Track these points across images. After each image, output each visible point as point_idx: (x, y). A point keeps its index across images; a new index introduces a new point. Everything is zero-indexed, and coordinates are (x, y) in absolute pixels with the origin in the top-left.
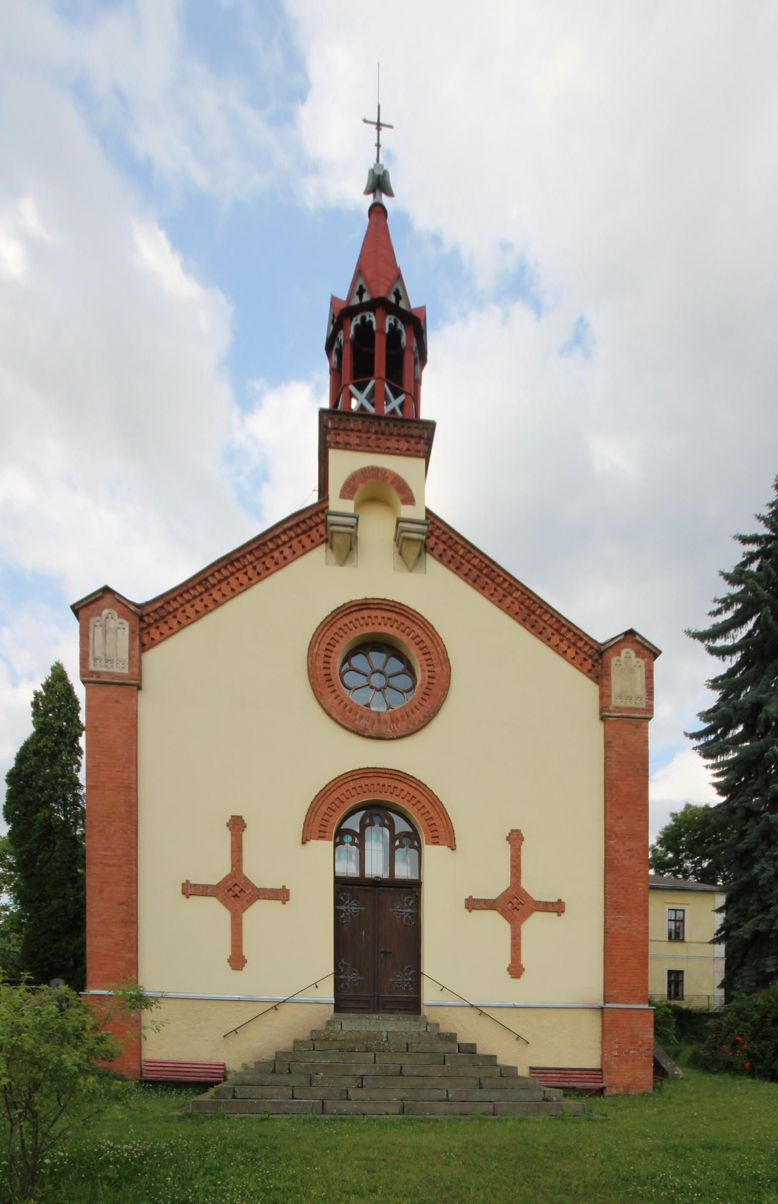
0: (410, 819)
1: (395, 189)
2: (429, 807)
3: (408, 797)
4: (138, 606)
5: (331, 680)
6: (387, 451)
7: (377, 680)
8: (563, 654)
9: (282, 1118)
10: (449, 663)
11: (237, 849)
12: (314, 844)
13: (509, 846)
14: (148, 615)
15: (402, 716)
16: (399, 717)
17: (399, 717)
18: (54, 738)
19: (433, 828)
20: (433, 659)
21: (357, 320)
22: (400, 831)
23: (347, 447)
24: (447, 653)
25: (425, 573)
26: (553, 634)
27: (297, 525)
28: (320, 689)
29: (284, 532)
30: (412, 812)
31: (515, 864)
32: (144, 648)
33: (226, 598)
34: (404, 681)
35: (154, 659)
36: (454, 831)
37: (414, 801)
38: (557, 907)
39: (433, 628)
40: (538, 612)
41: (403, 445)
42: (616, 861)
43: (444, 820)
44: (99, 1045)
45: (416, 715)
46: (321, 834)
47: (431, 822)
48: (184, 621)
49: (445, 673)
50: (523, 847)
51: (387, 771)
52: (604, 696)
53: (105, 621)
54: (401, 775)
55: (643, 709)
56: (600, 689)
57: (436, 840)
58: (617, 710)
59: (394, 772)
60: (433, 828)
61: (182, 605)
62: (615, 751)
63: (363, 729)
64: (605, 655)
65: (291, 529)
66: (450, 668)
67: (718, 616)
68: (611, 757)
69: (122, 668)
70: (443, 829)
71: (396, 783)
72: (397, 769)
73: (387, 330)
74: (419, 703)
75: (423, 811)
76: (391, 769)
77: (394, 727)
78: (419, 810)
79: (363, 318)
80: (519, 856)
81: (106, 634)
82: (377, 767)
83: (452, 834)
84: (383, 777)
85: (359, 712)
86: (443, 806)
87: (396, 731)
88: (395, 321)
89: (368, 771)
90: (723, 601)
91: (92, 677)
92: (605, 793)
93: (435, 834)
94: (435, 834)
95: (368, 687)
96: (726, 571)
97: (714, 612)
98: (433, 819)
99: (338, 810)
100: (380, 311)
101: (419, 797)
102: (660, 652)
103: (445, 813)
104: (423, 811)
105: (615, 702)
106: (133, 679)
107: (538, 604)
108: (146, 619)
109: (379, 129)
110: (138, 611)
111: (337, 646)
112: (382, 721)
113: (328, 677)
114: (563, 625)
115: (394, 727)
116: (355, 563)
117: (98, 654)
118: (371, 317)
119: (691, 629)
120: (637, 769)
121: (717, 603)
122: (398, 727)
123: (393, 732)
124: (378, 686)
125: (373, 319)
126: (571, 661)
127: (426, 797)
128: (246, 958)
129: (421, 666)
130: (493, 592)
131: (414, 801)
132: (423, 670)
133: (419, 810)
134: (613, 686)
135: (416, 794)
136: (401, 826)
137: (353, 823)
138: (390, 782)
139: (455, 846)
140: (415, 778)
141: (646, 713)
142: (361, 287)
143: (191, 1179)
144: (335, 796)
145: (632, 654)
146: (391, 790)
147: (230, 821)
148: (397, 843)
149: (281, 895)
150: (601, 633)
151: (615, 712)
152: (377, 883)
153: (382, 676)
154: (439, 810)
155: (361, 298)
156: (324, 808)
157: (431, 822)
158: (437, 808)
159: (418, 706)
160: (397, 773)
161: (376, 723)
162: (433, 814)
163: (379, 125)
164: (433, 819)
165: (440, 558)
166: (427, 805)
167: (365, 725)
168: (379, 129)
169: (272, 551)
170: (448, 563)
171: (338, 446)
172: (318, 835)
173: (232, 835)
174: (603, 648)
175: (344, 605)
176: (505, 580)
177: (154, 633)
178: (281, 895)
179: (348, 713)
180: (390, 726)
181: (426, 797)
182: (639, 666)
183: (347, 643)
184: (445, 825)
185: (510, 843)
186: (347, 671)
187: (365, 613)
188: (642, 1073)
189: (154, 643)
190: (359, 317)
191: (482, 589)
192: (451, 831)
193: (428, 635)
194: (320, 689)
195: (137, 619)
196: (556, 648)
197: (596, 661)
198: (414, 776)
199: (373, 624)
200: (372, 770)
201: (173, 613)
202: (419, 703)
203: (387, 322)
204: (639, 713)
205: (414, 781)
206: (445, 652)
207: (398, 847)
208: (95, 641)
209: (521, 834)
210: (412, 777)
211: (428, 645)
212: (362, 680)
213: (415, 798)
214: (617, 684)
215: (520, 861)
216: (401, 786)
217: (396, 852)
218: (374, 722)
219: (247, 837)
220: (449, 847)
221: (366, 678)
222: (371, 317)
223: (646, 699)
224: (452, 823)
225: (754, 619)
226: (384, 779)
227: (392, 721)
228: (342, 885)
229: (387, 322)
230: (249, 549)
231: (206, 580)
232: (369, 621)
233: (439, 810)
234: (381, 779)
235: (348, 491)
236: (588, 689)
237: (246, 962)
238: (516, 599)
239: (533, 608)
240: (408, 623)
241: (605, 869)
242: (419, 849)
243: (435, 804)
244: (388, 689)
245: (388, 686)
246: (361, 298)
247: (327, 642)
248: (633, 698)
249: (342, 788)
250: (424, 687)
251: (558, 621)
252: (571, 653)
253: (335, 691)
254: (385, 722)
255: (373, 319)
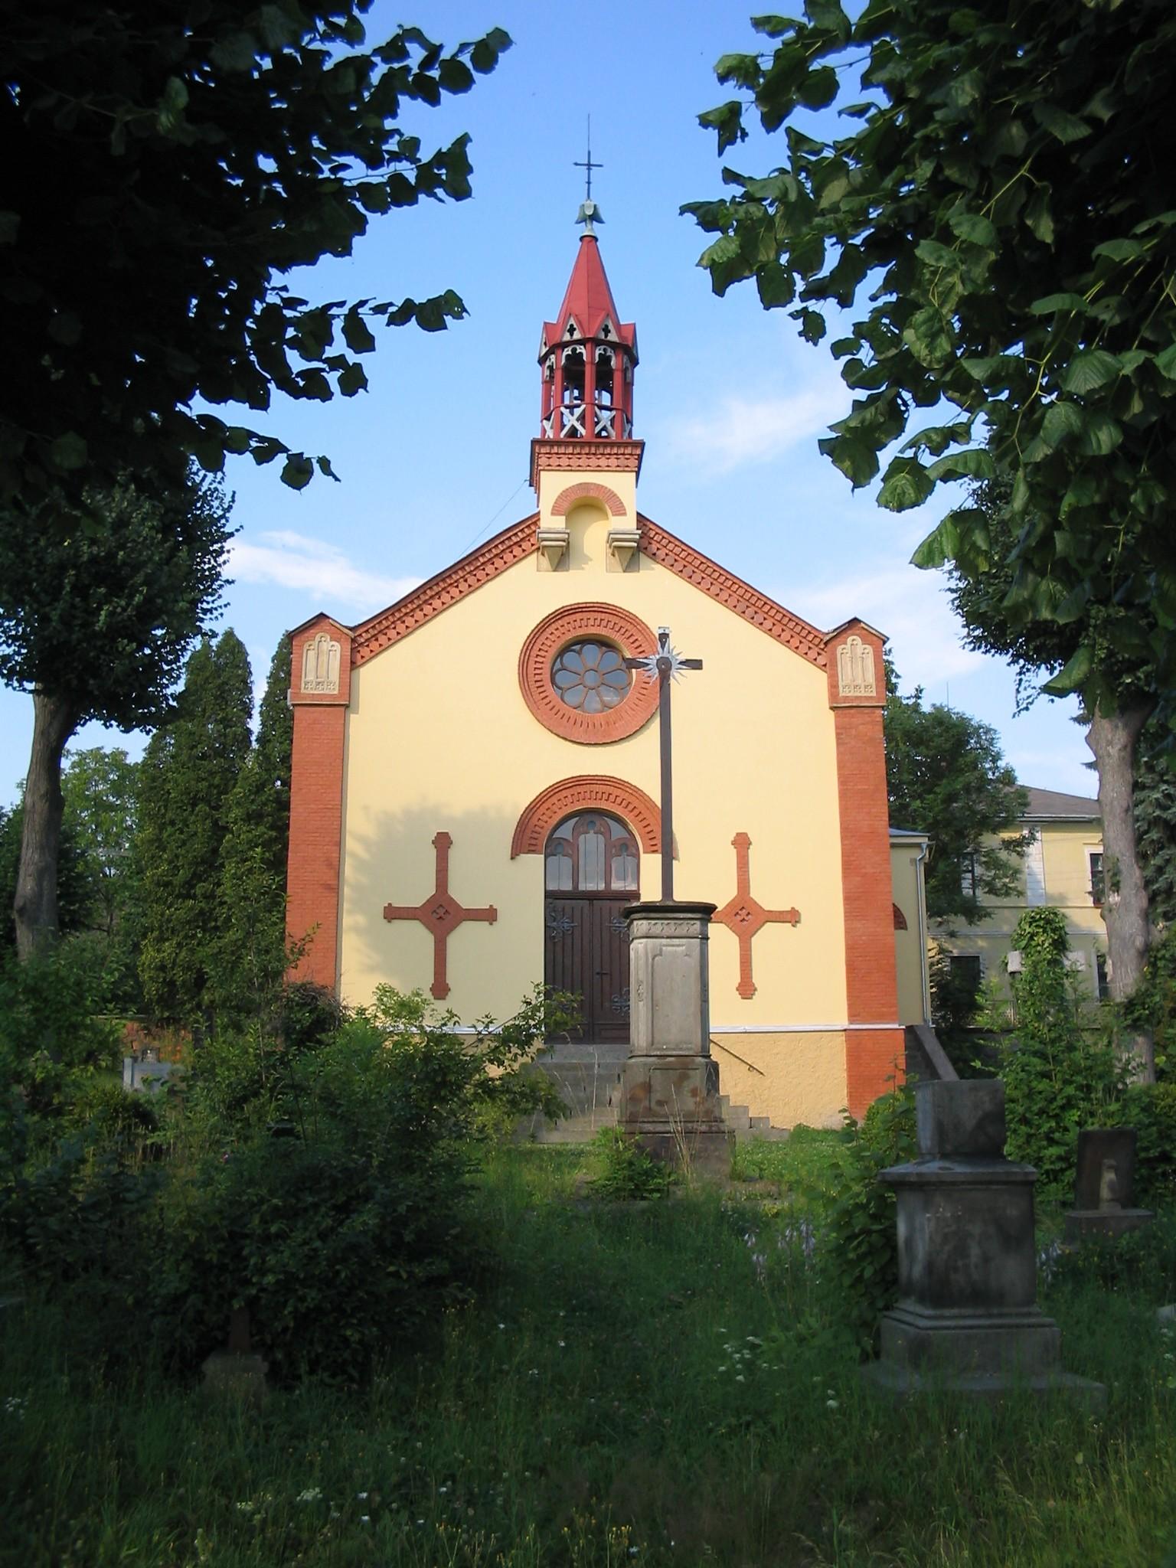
0: (609, 641)
1: (603, 218)
4: (351, 629)
6: (599, 469)
7: (590, 679)
12: (525, 858)
14: (360, 635)
18: (1071, 131)
21: (568, 351)
35: (369, 674)
38: (792, 917)
48: (457, 596)
52: (833, 686)
69: (332, 688)
73: (597, 360)
79: (574, 350)
88: (605, 350)
100: (589, 346)
109: (589, 169)
118: (580, 349)
125: (584, 351)
128: (450, 986)
137: (565, 832)
142: (572, 326)
145: (858, 640)
149: (489, 915)
152: (592, 897)
155: (572, 335)
163: (589, 166)
168: (589, 169)
171: (549, 468)
177: (365, 651)
178: (489, 915)
186: (560, 670)
190: (570, 348)
203: (597, 352)
219: (453, 854)
222: (580, 349)
228: (552, 897)
229: (597, 352)
237: (444, 999)
244: (603, 688)
246: (572, 335)
255: (584, 351)
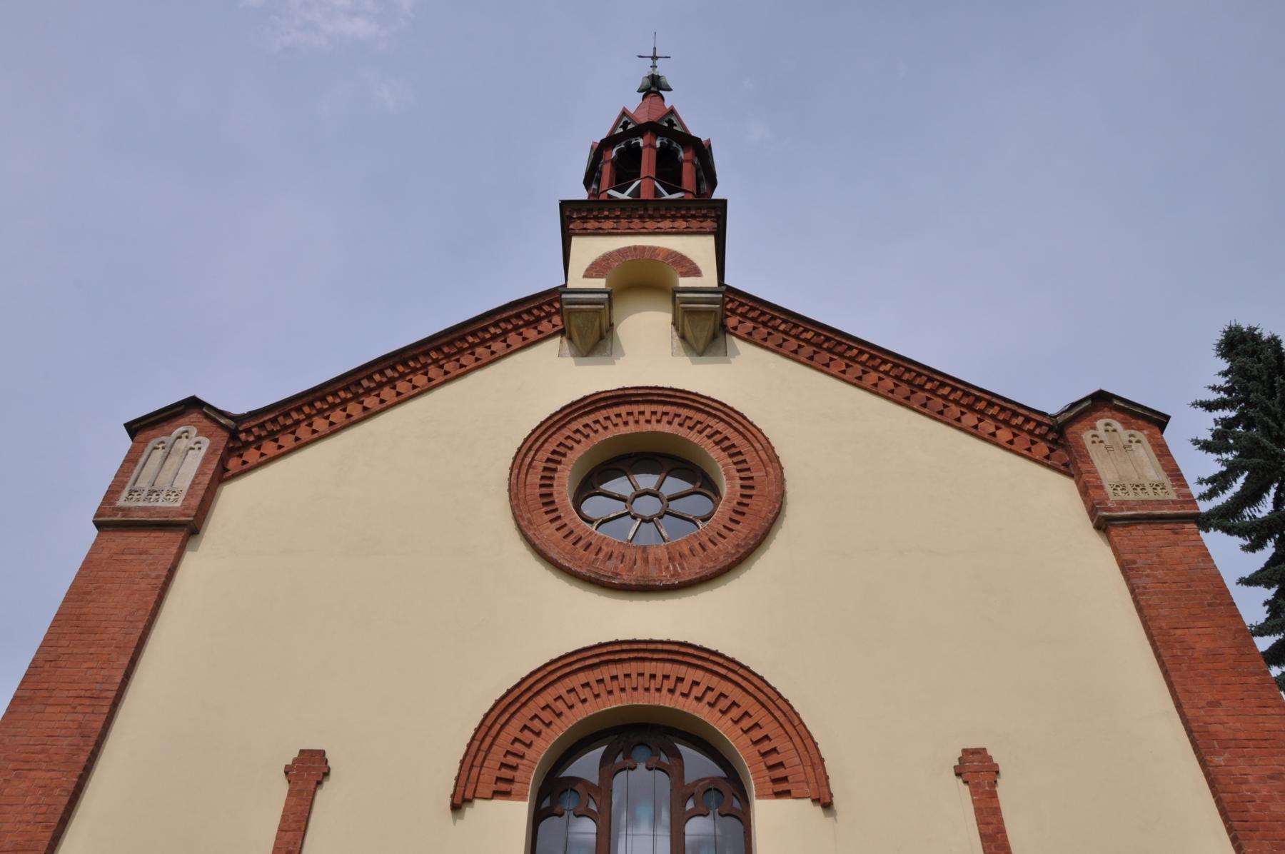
2: (758, 714)
3: (710, 697)
5: (553, 502)
7: (648, 506)
8: (991, 439)
10: (779, 462)
11: (294, 826)
13: (966, 789)
15: (691, 550)
16: (686, 551)
17: (686, 551)
19: (773, 760)
20: (747, 460)
22: (695, 779)
24: (773, 448)
25: (726, 355)
26: (963, 413)
27: (518, 316)
28: (529, 515)
29: (496, 325)
30: (723, 726)
31: (990, 830)
33: (385, 407)
34: (696, 505)
36: (822, 760)
37: (724, 704)
39: (745, 418)
40: (928, 386)
42: (1250, 806)
43: (797, 739)
45: (720, 546)
46: (503, 787)
47: (766, 746)
49: (772, 476)
50: (1000, 790)
51: (660, 647)
52: (1089, 490)
53: (175, 441)
54: (691, 651)
55: (1173, 502)
56: (1077, 483)
57: (783, 787)
58: (1124, 507)
59: (676, 648)
60: (773, 760)
61: (309, 417)
62: (1148, 576)
63: (610, 574)
64: (1070, 432)
65: (507, 320)
66: (781, 468)
67: (1214, 499)
68: (1145, 588)
70: (797, 760)
71: (682, 671)
72: (682, 640)
74: (725, 527)
75: (746, 723)
76: (668, 642)
77: (674, 567)
78: (736, 722)
80: (997, 811)
81: (167, 457)
82: (638, 638)
83: (819, 770)
84: (652, 660)
85: (604, 547)
86: (791, 707)
87: (679, 575)
89: (617, 648)
90: (1212, 480)
91: (116, 515)
92: (1158, 656)
93: (779, 773)
94: (779, 773)
95: (629, 517)
96: (1201, 438)
97: (1205, 494)
98: (770, 740)
99: (557, 721)
101: (734, 693)
102: (1168, 418)
103: (796, 722)
104: (746, 723)
106: (185, 515)
107: (925, 375)
108: (243, 436)
110: (231, 423)
111: (568, 455)
112: (651, 558)
113: (548, 500)
114: (978, 399)
115: (674, 567)
116: (608, 352)
117: (143, 484)
119: (1216, 384)
120: (1210, 605)
121: (1204, 484)
122: (683, 568)
123: (672, 576)
124: (647, 514)
127: (750, 694)
129: (727, 473)
130: (844, 368)
131: (724, 704)
132: (730, 478)
133: (736, 722)
134: (1099, 470)
135: (727, 688)
136: (697, 765)
137: (587, 766)
138: (668, 668)
139: (831, 795)
140: (722, 656)
141: (1183, 508)
144: (541, 701)
146: (669, 684)
147: (295, 761)
148: (690, 805)
150: (1052, 402)
151: (1122, 510)
153: (657, 499)
154: (782, 719)
156: (513, 729)
157: (766, 746)
158: (778, 714)
159: (725, 532)
160: (683, 649)
161: (639, 564)
162: (770, 728)
164: (770, 740)
165: (748, 338)
166: (755, 709)
167: (616, 568)
169: (473, 346)
170: (762, 344)
172: (494, 787)
173: (290, 794)
174: (1060, 420)
175: (585, 398)
176: (861, 352)
179: (582, 551)
180: (667, 568)
181: (750, 694)
182: (1138, 442)
183: (585, 450)
184: (802, 750)
185: (966, 782)
187: (623, 410)
191: (824, 368)
192: (816, 761)
193: (736, 430)
194: (529, 515)
195: (226, 435)
197: (1054, 442)
198: (720, 651)
199: (623, 690)
200: (625, 647)
201: (292, 428)
202: (725, 527)
204: (1169, 509)
205: (721, 661)
206: (768, 447)
207: (693, 814)
208: (145, 468)
209: (990, 758)
210: (716, 653)
211: (736, 443)
212: (620, 507)
213: (726, 697)
215: (1001, 822)
216: (691, 675)
218: (635, 563)
220: (816, 801)
221: (624, 504)
223: (1173, 486)
224: (815, 744)
225: (1273, 491)
226: (654, 664)
227: (671, 559)
230: (435, 344)
231: (358, 384)
232: (615, 686)
233: (782, 719)
234: (647, 664)
238: (886, 373)
239: (918, 381)
240: (698, 416)
241: (1230, 830)
242: (744, 818)
243: (771, 707)
245: (666, 513)
247: (551, 449)
248: (1147, 486)
249: (559, 685)
250: (735, 502)
251: (966, 394)
252: (1004, 435)
253: (559, 518)
254: (658, 561)
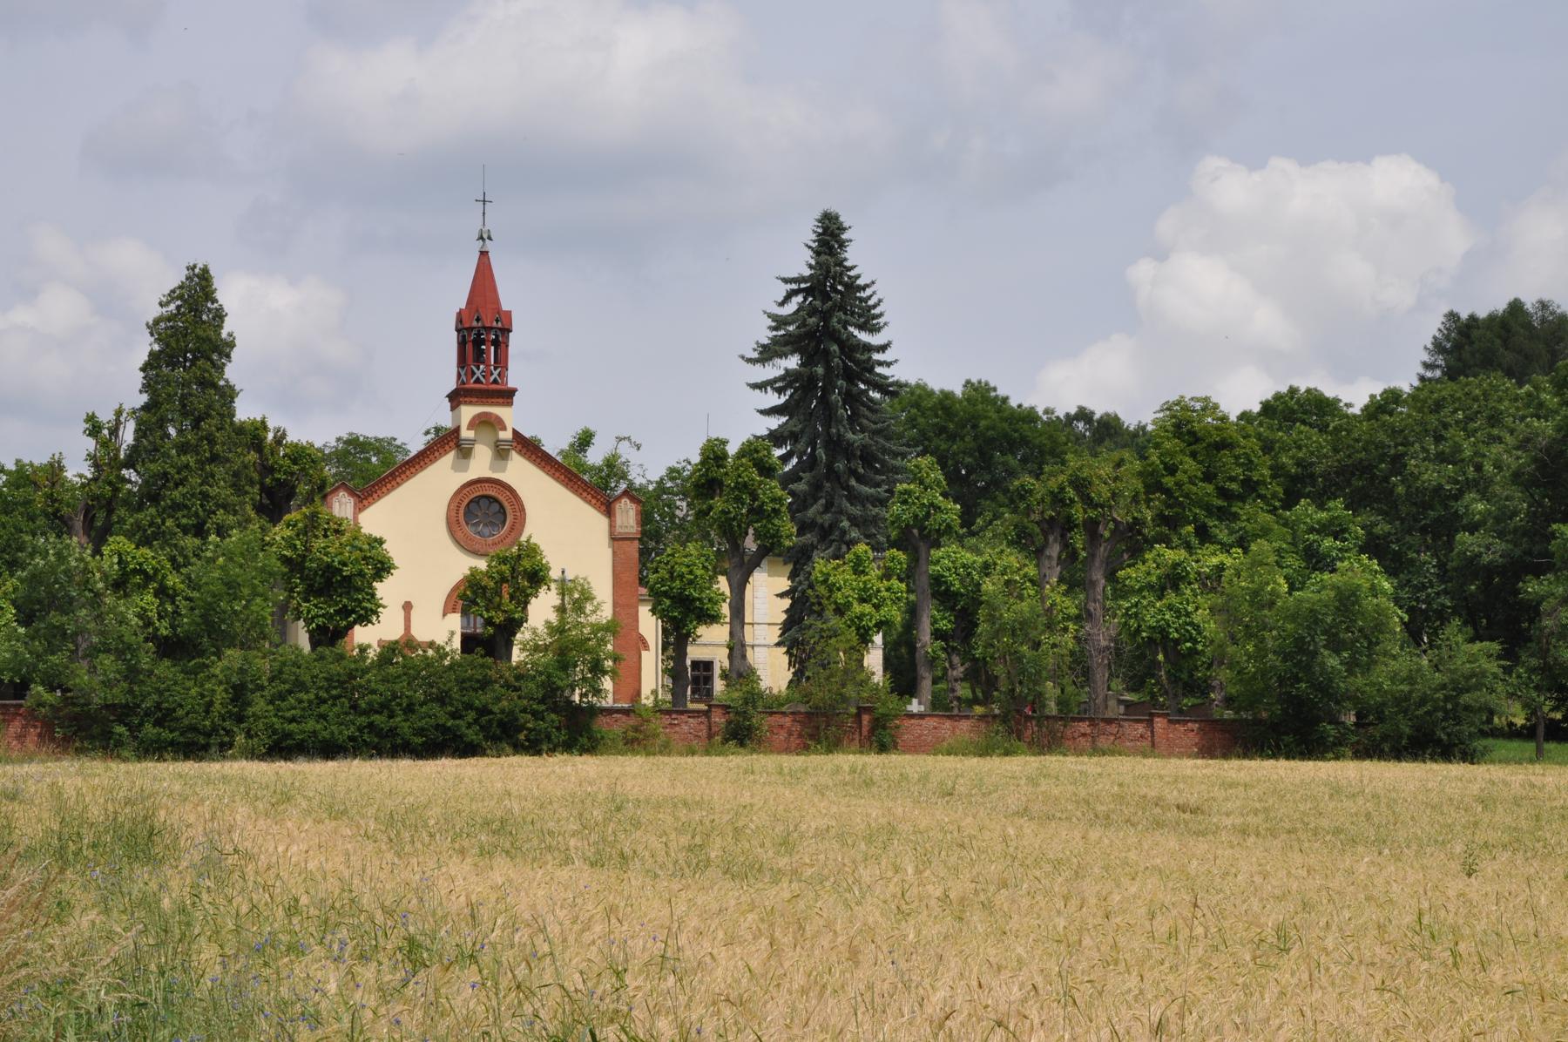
6: (492, 404)
9: (924, 778)
23: (471, 403)
32: (361, 510)
41: (501, 400)
44: (1446, 440)
52: (612, 526)
105: (618, 530)
126: (594, 506)
143: (908, 915)
188: (1420, 712)
189: (365, 508)
196: (585, 499)
214: (619, 520)
217: (1430, 179)
235: (471, 426)
236: (601, 522)
252: (594, 501)
